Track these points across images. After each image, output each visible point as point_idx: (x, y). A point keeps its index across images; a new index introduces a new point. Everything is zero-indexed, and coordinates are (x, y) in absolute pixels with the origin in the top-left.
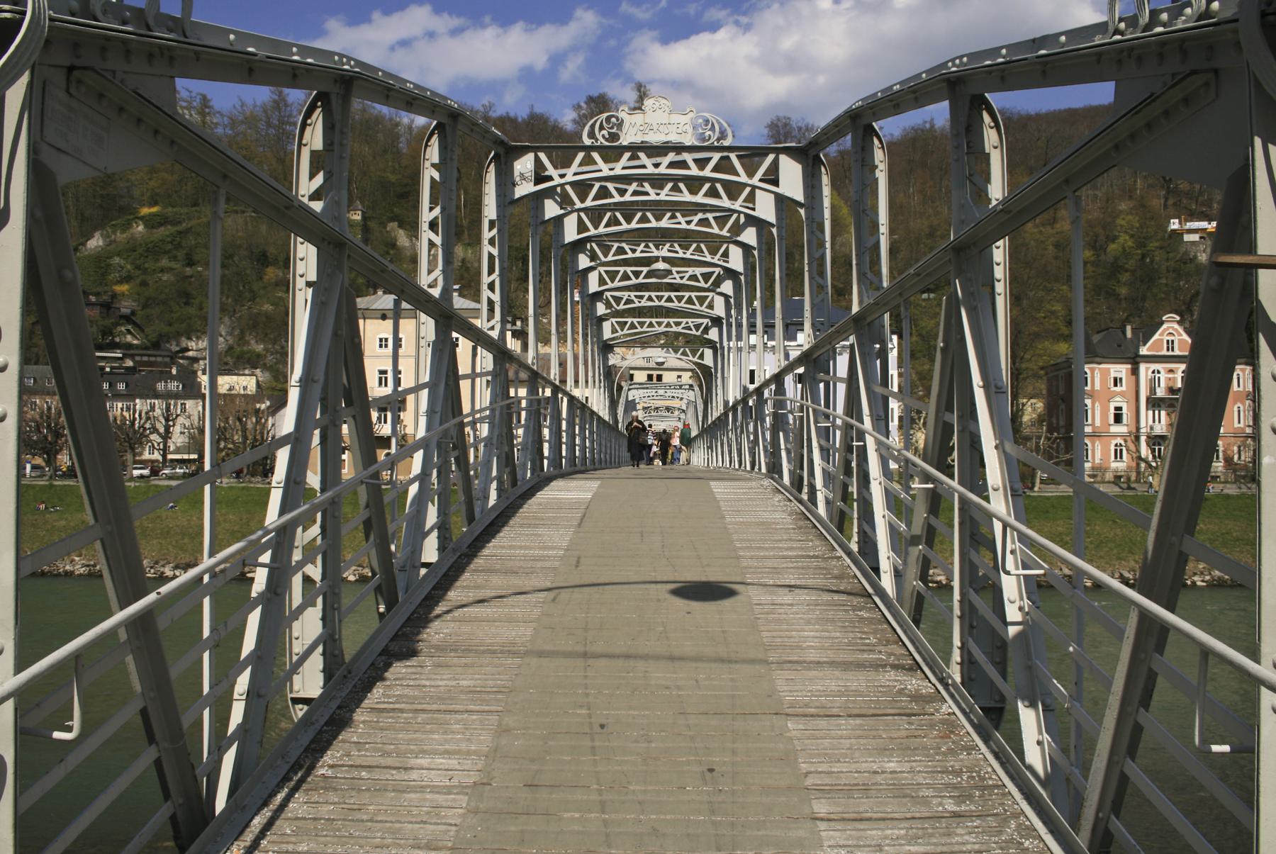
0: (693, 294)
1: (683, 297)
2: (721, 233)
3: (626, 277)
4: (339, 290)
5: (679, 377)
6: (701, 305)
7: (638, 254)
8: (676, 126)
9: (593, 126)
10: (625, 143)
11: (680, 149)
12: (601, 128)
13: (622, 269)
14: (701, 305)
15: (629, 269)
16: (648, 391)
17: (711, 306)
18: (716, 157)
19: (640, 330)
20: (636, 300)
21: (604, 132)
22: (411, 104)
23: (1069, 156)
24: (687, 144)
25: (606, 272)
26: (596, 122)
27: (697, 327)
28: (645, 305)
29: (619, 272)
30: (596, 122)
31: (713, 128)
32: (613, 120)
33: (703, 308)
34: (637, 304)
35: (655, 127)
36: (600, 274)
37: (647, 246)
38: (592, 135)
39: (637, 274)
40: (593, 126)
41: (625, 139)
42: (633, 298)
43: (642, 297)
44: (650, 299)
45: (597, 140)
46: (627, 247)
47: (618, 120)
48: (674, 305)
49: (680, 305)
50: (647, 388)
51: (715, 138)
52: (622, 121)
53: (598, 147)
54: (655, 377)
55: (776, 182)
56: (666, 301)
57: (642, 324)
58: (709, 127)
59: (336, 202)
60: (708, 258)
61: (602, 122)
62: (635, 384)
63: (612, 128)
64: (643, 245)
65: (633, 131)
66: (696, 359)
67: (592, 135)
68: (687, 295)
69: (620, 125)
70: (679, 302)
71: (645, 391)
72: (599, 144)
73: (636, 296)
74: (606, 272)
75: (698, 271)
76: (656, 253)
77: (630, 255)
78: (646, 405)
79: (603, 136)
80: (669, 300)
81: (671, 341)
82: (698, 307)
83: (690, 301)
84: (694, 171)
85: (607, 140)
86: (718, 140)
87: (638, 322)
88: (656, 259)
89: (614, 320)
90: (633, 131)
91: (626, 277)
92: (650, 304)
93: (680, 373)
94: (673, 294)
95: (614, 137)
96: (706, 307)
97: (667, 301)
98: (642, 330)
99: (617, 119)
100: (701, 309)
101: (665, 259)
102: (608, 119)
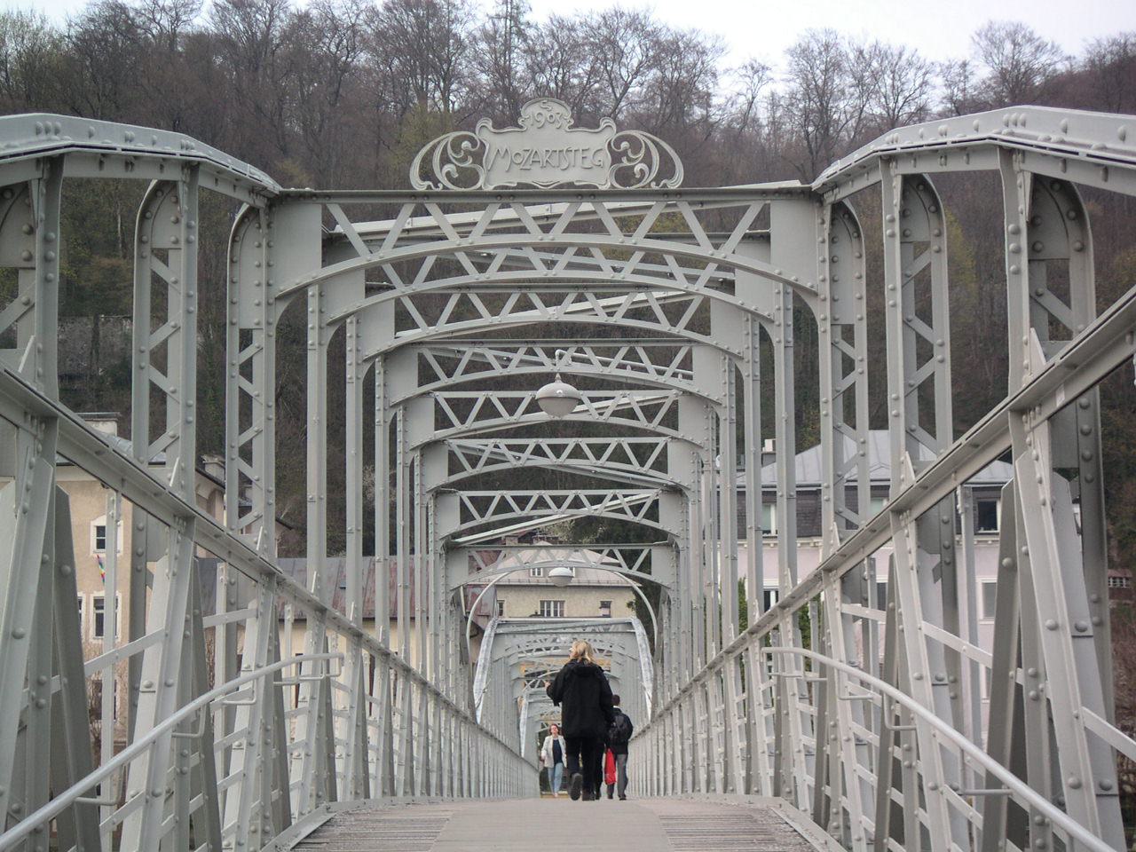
0: (625, 442)
1: (606, 446)
2: (675, 331)
3: (488, 411)
4: (48, 499)
5: (605, 605)
6: (642, 464)
7: (513, 370)
8: (580, 155)
9: (427, 160)
10: (490, 188)
11: (592, 194)
12: (445, 160)
13: (481, 396)
14: (642, 464)
15: (495, 396)
16: (539, 637)
17: (661, 465)
18: (656, 209)
19: (518, 513)
20: (509, 454)
21: (448, 168)
22: (132, 164)
23: (1030, 385)
24: (601, 188)
25: (471, 499)
26: (434, 148)
27: (636, 509)
28: (530, 464)
29: (475, 400)
30: (434, 148)
31: (648, 160)
32: (466, 144)
33: (645, 469)
34: (514, 464)
35: (543, 157)
36: (437, 403)
37: (531, 352)
38: (427, 174)
39: (511, 406)
40: (427, 160)
41: (487, 181)
42: (504, 450)
43: (522, 449)
44: (538, 451)
45: (436, 182)
46: (490, 355)
47: (474, 145)
48: (589, 464)
49: (599, 463)
50: (535, 632)
51: (653, 175)
52: (483, 145)
53: (438, 195)
54: (552, 615)
55: (664, 469)
56: (570, 457)
57: (522, 502)
58: (641, 155)
59: (182, 469)
60: (652, 376)
61: (445, 149)
62: (507, 623)
63: (464, 160)
64: (523, 350)
65: (503, 164)
66: (634, 572)
67: (427, 174)
68: (613, 442)
69: (478, 156)
70: (598, 457)
71: (532, 637)
72: (440, 189)
73: (510, 447)
74: (471, 499)
75: (635, 398)
76: (548, 367)
77: (498, 371)
78: (532, 670)
79: (448, 174)
80: (577, 453)
81: (585, 532)
82: (636, 466)
83: (619, 455)
84: (616, 238)
85: (454, 182)
86: (657, 180)
87: (502, 400)
88: (549, 378)
89: (465, 494)
90: (503, 164)
91: (488, 411)
92: (539, 462)
93: (605, 597)
94: (584, 442)
95: (468, 177)
96: (652, 467)
97: (573, 455)
98: (524, 514)
99: (472, 140)
100: (643, 470)
101: (566, 378)
102: (456, 145)
